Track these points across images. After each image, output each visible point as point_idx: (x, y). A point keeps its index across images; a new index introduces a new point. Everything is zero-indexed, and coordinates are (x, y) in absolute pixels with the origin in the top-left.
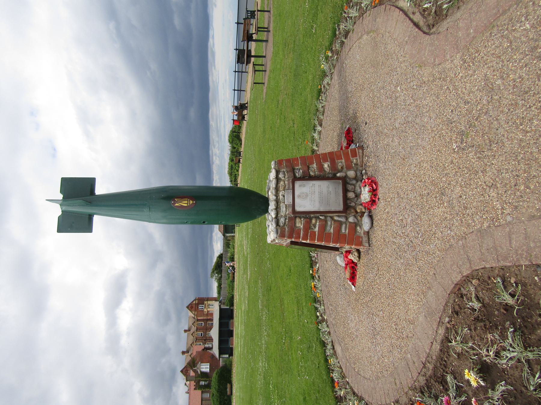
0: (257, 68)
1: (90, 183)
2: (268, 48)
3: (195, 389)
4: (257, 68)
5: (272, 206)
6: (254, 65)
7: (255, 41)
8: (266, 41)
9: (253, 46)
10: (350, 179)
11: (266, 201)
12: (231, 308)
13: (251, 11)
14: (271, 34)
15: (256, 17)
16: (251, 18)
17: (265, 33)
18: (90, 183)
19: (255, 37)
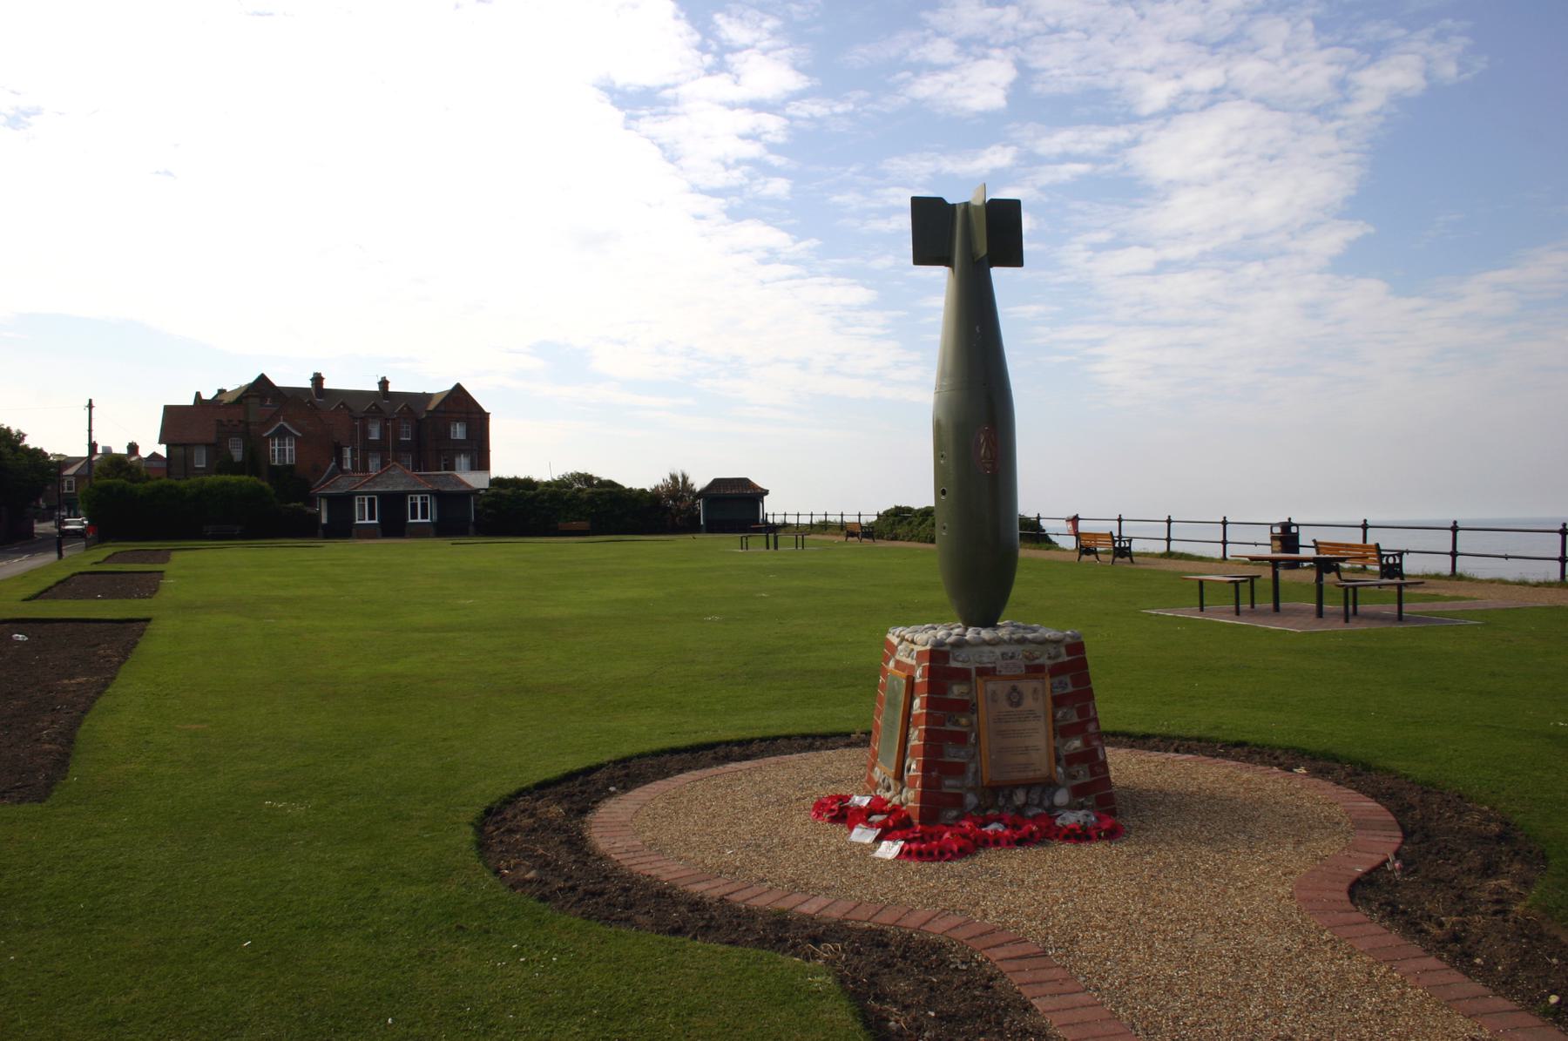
0: (1245, 590)
1: (1013, 257)
2: (1548, 591)
3: (220, 423)
4: (1245, 590)
5: (986, 634)
6: (1252, 578)
7: (1319, 578)
8: (1320, 613)
9: (1308, 576)
10: (1053, 794)
11: (990, 622)
12: (471, 528)
13: (1400, 565)
14: (1339, 626)
15: (1386, 581)
16: (1382, 566)
17: (1342, 608)
18: (1013, 257)
19: (1330, 578)
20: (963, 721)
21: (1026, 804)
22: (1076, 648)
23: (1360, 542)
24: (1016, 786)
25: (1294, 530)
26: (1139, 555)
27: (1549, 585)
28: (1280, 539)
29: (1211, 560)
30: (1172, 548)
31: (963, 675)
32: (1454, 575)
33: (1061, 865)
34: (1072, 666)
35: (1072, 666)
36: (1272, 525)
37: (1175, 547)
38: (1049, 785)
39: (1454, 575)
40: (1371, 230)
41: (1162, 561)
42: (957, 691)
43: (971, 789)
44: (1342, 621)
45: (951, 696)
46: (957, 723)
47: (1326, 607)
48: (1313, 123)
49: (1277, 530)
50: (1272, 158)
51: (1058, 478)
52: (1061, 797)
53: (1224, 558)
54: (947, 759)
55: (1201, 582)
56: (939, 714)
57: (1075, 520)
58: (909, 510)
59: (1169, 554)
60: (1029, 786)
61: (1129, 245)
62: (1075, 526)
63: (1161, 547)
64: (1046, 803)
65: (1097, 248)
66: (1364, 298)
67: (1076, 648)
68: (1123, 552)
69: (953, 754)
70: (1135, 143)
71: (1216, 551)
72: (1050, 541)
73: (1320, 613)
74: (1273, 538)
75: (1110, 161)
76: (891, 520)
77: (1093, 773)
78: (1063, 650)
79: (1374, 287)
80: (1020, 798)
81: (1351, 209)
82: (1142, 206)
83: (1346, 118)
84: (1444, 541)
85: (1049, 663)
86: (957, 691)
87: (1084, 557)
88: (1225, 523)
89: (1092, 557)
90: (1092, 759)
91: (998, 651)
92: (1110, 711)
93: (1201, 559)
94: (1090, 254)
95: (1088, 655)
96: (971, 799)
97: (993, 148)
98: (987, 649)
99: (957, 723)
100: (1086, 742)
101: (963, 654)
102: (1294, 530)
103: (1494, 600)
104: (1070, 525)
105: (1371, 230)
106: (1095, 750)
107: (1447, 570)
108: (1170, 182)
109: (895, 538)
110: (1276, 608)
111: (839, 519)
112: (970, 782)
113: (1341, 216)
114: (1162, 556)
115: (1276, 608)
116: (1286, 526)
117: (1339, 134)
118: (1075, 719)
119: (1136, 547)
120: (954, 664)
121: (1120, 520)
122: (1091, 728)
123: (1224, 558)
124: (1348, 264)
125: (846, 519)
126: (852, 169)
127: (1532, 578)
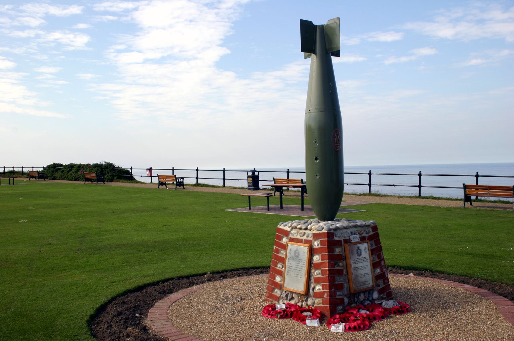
11: (331, 218)
20: (341, 264)
21: (364, 300)
22: (375, 228)
23: (286, 178)
24: (359, 293)
25: (256, 173)
26: (186, 185)
27: (365, 195)
28: (252, 177)
29: (218, 187)
30: (199, 182)
31: (339, 243)
32: (370, 194)
33: (429, 328)
34: (373, 237)
35: (373, 237)
36: (248, 172)
37: (200, 181)
38: (370, 291)
39: (370, 194)
40: (229, 52)
41: (195, 187)
42: (338, 251)
43: (345, 296)
44: (300, 211)
45: (336, 253)
46: (339, 266)
47: (284, 205)
48: (205, 9)
49: (250, 174)
50: (191, 21)
51: (367, 154)
52: (375, 295)
53: (224, 186)
54: (337, 283)
55: (249, 197)
56: (332, 262)
57: (150, 169)
58: (61, 165)
59: (197, 185)
60: (364, 292)
61: (133, 51)
62: (151, 173)
63: (194, 181)
64: (370, 299)
65: (119, 51)
66: (226, 78)
67: (375, 228)
68: (180, 184)
69: (339, 280)
70: (136, 9)
71: (220, 183)
72: (134, 179)
73: (302, 209)
74: (248, 177)
75: (126, 16)
76: (51, 170)
77: (385, 283)
78: (371, 229)
79: (231, 74)
80: (362, 297)
81: (226, 42)
82: (138, 36)
83: (219, 9)
84: (365, 179)
85: (367, 235)
86: (338, 251)
87: (161, 186)
88: (197, 170)
89: (164, 186)
90: (382, 277)
91: (349, 231)
92: (389, 257)
93: (213, 186)
94: (116, 54)
95: (379, 231)
96: (346, 300)
97: (73, 6)
98: (345, 230)
99: (339, 266)
100: (382, 270)
101: (338, 233)
102: (256, 173)
103: (396, 201)
104: (148, 172)
105: (229, 52)
106: (384, 273)
107: (367, 191)
108: (150, 27)
109: (54, 179)
110: (281, 207)
111: (21, 170)
112: (346, 292)
113: (221, 46)
114: (194, 185)
115: (281, 207)
116: (254, 172)
117: (217, 14)
118: (377, 260)
119: (186, 181)
120: (336, 238)
121: (420, 175)
122: (382, 263)
123: (224, 186)
124: (222, 64)
125: (15, 169)
126: (7, 7)
127: (358, 192)
